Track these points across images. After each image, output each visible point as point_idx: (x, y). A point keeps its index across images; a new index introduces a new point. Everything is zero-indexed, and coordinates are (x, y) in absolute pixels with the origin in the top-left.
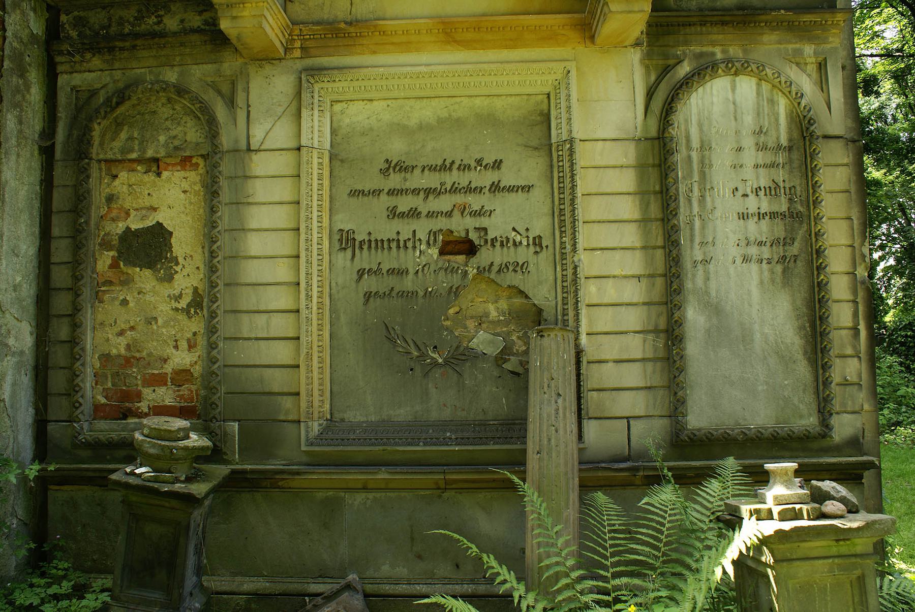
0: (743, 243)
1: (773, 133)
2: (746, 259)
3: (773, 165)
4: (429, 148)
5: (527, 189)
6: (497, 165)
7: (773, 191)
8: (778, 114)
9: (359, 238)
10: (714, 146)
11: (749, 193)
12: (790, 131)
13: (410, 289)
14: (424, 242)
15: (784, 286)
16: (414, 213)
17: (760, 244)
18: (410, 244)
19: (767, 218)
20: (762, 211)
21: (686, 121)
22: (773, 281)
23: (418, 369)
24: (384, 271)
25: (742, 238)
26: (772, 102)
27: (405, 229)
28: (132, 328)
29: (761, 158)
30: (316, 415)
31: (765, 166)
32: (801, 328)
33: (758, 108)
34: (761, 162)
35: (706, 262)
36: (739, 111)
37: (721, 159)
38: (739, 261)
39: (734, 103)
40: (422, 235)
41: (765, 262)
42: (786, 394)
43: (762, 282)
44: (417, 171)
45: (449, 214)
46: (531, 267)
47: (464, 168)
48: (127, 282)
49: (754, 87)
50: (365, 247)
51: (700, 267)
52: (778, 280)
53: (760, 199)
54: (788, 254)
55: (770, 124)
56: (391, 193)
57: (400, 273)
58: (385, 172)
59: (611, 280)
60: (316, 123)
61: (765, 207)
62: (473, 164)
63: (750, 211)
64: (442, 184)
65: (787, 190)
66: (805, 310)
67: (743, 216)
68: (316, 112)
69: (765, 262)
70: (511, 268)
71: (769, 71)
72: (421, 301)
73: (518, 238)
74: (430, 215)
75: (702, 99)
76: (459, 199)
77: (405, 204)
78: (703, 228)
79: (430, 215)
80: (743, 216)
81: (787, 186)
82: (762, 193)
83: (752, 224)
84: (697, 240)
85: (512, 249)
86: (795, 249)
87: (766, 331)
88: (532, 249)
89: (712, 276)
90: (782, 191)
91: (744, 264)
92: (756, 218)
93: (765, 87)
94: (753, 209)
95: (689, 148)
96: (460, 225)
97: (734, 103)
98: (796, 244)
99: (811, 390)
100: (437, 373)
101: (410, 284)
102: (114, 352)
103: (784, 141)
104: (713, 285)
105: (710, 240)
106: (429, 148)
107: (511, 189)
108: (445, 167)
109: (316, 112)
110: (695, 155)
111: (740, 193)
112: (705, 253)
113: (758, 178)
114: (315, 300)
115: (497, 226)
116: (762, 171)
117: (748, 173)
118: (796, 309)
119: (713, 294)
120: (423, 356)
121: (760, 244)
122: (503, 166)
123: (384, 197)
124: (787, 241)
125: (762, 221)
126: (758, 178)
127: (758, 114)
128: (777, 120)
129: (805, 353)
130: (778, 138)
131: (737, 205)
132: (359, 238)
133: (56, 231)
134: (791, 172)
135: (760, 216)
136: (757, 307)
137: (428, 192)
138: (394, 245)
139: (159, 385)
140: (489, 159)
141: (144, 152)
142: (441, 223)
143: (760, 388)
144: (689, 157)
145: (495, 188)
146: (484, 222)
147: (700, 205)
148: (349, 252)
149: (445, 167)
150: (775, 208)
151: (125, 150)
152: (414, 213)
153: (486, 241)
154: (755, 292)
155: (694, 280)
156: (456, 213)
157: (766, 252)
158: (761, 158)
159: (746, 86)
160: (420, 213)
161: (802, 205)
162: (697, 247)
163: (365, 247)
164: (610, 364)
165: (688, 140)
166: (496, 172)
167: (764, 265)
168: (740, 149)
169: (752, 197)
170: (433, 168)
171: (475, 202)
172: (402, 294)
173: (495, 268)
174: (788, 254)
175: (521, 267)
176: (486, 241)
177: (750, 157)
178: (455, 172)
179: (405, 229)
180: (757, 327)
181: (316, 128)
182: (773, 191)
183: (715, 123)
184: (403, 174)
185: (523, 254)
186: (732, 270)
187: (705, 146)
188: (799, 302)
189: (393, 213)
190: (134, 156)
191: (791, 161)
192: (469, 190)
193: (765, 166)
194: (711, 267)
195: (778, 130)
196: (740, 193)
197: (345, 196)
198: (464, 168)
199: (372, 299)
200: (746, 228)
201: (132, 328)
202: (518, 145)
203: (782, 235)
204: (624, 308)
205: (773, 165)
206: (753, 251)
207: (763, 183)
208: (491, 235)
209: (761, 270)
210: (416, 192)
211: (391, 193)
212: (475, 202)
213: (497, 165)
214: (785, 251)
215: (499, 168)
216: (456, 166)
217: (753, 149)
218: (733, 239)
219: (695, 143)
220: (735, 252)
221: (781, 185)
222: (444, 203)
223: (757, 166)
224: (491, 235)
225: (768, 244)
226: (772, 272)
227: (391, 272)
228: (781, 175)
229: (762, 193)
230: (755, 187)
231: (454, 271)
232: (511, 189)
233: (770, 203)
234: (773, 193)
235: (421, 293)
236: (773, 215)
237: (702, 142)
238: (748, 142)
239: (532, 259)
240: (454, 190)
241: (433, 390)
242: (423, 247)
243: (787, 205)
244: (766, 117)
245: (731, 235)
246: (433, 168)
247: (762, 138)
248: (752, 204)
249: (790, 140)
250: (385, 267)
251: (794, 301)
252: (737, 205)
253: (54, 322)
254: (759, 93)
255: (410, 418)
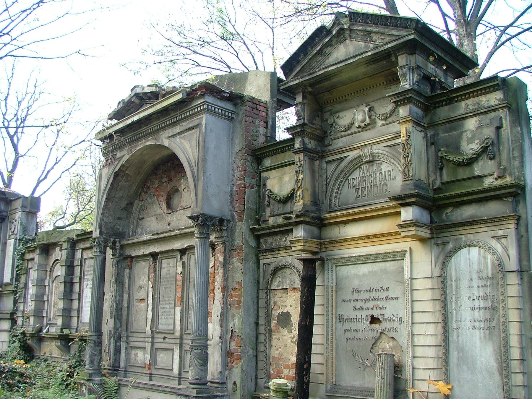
0: (473, 321)
1: (485, 272)
2: (474, 328)
3: (485, 286)
4: (366, 283)
5: (397, 298)
6: (387, 289)
7: (485, 297)
8: (487, 263)
9: (345, 318)
10: (461, 278)
11: (475, 299)
12: (492, 269)
13: (360, 337)
14: (365, 319)
15: (489, 340)
16: (361, 308)
17: (480, 321)
18: (360, 320)
19: (483, 309)
20: (481, 307)
21: (450, 269)
22: (485, 337)
23: (362, 368)
24: (352, 330)
25: (473, 319)
26: (485, 258)
27: (359, 314)
28: (280, 348)
29: (481, 283)
30: (329, 382)
31: (482, 286)
32: (497, 359)
33: (479, 261)
34: (480, 285)
35: (458, 329)
36: (471, 263)
37: (464, 284)
38: (471, 328)
39: (469, 260)
40: (364, 317)
41: (482, 329)
42: (490, 388)
43: (480, 338)
44: (362, 292)
45: (372, 309)
46: (398, 330)
47: (377, 290)
48: (279, 332)
49: (477, 251)
50: (347, 321)
51: (455, 331)
52: (487, 337)
53: (480, 301)
54: (491, 326)
55: (484, 267)
56: (354, 300)
57: (357, 331)
58: (352, 293)
59: (422, 336)
60: (330, 275)
61: (482, 305)
62: (380, 289)
63: (476, 307)
64: (370, 297)
65: (491, 297)
66: (498, 351)
67: (473, 309)
68: (330, 272)
69: (482, 329)
70: (392, 330)
71: (481, 244)
72: (363, 342)
73: (394, 318)
74: (367, 309)
75: (457, 259)
76: (375, 303)
77: (359, 305)
78: (456, 314)
79: (367, 309)
80: (473, 309)
81: (491, 295)
82: (480, 299)
83: (476, 313)
84: (454, 320)
85: (392, 322)
86: (494, 324)
87: (482, 359)
88: (399, 323)
89: (460, 335)
90: (489, 297)
91: (473, 330)
92: (478, 310)
93: (482, 251)
94: (477, 306)
95: (452, 281)
96: (376, 313)
97: (469, 260)
98: (494, 321)
99: (501, 387)
100: (368, 369)
101: (360, 335)
102: (276, 356)
103: (490, 275)
104: (461, 339)
105: (459, 319)
106: (366, 283)
107: (392, 299)
108: (371, 291)
109: (330, 272)
110: (453, 283)
111: (472, 299)
112: (457, 325)
113: (479, 292)
114: (330, 340)
115: (388, 313)
116: (480, 288)
117: (475, 290)
118: (495, 351)
119: (461, 343)
120: (363, 363)
121: (480, 321)
122: (389, 289)
123: (352, 302)
124: (491, 320)
125: (481, 311)
126: (479, 292)
127: (479, 264)
128: (487, 266)
129: (498, 370)
130: (487, 274)
131: (470, 304)
132: (345, 318)
133: (260, 314)
134: (493, 289)
135: (480, 309)
136: (479, 349)
137: (366, 300)
138: (355, 320)
139: (287, 368)
140: (385, 288)
141: (283, 286)
142: (370, 313)
143: (479, 384)
144: (451, 284)
145: (387, 298)
146: (383, 312)
147: (455, 305)
148: (342, 322)
149: (371, 291)
150: (486, 305)
151: (278, 286)
152: (361, 308)
153: (384, 319)
154: (478, 342)
155: (453, 337)
156: (375, 308)
157: (482, 325)
158: (481, 283)
159: (474, 251)
160: (363, 308)
161: (497, 304)
162: (454, 322)
163: (347, 321)
164: (422, 370)
165: (451, 277)
166: (387, 292)
167: (482, 331)
168: (471, 280)
169: (476, 300)
170: (367, 291)
171: (380, 304)
172: (358, 339)
173: (387, 330)
174: (491, 326)
175: (395, 330)
176: (384, 319)
177: (476, 283)
178: (374, 292)
179: (359, 314)
180: (478, 357)
181: (330, 277)
182: (485, 297)
183: (461, 269)
184: (358, 293)
185: (396, 325)
186: (468, 332)
187: (458, 279)
188: (496, 347)
189: (355, 309)
190: (280, 288)
191: (493, 284)
192: (378, 299)
193: (482, 286)
194: (460, 331)
195: (487, 270)
196: (472, 299)
197: (340, 302)
198: (377, 290)
199: (348, 341)
200: (474, 314)
201: (280, 348)
202: (394, 281)
203: (488, 317)
204: (427, 347)
205: (485, 286)
206: (477, 324)
207: (481, 294)
208: (385, 317)
209: (480, 332)
210: (362, 300)
211: (354, 300)
212: (380, 304)
213: (387, 289)
214: (490, 324)
215: (388, 290)
216: (374, 290)
217: (477, 279)
218: (468, 319)
219: (454, 279)
220: (469, 324)
221: (489, 295)
222: (370, 304)
223: (478, 287)
224: (385, 317)
225: (483, 321)
226: (485, 334)
227: (355, 330)
228: (488, 290)
229: (480, 299)
230: (478, 296)
231: (374, 330)
232: (392, 299)
233: (484, 303)
234: (485, 298)
235: (364, 339)
236: (485, 308)
237: (456, 277)
238: (475, 276)
239: (399, 326)
240: (374, 299)
241: (366, 376)
242: (364, 321)
243: (491, 304)
244: (482, 265)
245: (467, 317)
246: (367, 291)
247: (481, 274)
248: (476, 304)
249: (492, 274)
250: (353, 329)
251: (494, 348)
252: (470, 304)
253: (260, 345)
254: (479, 254)
255: (359, 386)
